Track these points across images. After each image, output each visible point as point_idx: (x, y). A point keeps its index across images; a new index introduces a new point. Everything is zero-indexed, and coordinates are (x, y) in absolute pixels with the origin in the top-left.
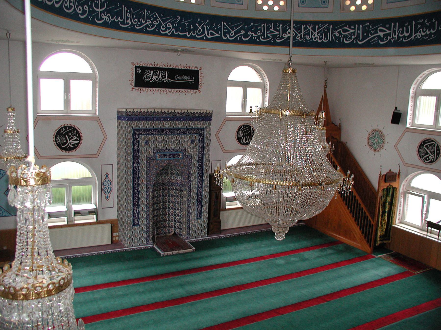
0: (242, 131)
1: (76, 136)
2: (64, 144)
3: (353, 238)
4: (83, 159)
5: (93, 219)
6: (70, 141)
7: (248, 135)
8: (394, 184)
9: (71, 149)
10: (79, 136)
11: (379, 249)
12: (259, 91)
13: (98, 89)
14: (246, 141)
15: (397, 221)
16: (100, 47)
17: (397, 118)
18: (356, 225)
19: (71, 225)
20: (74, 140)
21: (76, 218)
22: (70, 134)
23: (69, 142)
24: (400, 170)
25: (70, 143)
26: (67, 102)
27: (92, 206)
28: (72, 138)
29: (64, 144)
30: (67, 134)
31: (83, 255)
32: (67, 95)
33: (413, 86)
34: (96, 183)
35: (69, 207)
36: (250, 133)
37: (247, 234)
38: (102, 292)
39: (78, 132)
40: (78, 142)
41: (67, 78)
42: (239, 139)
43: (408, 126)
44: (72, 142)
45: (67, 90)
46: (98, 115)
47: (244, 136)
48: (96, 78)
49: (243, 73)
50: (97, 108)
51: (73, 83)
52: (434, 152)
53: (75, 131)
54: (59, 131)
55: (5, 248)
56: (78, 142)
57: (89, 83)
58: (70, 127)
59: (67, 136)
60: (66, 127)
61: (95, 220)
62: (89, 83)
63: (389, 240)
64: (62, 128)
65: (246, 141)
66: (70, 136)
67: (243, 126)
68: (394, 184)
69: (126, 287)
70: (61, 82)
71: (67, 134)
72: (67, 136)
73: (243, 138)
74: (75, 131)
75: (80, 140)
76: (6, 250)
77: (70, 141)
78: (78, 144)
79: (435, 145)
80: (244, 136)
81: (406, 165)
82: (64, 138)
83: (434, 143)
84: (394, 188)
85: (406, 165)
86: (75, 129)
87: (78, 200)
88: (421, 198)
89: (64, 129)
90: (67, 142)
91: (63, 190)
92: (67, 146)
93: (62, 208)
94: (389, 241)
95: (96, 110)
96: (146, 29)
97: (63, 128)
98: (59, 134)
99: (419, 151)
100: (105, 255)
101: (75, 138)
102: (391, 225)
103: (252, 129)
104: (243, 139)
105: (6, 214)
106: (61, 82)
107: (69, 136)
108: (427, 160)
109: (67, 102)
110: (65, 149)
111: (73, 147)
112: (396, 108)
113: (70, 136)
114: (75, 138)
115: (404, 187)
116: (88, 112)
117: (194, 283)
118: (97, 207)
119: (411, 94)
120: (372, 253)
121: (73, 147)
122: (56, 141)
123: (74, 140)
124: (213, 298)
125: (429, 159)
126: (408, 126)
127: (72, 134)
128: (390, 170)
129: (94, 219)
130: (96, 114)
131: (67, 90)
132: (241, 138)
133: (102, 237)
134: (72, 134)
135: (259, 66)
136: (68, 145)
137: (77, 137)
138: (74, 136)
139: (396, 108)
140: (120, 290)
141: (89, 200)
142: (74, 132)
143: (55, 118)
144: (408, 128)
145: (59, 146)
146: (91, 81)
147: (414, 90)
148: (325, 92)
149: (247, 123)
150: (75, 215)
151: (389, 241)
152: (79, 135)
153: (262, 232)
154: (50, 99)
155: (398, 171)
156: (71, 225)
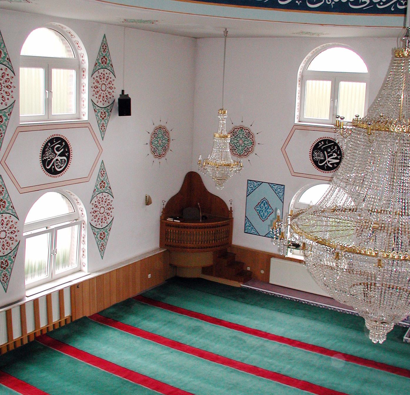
1: (336, 153)
2: (322, 161)
6: (329, 159)
9: (329, 169)
10: (340, 155)
12: (361, 88)
16: (355, 38)
20: (333, 159)
22: (329, 150)
23: (327, 160)
25: (329, 161)
28: (332, 155)
29: (322, 161)
30: (326, 149)
31: (343, 311)
38: (285, 348)
39: (339, 148)
40: (338, 161)
44: (331, 160)
49: (340, 58)
53: (336, 147)
54: (317, 145)
55: (249, 269)
56: (338, 161)
58: (330, 141)
59: (325, 152)
60: (325, 141)
64: (320, 142)
66: (329, 152)
69: (305, 352)
70: (328, 84)
71: (326, 149)
72: (325, 152)
74: (336, 147)
75: (340, 159)
76: (248, 271)
77: (329, 159)
78: (338, 164)
82: (322, 155)
86: (336, 144)
88: (58, 231)
89: (322, 142)
90: (325, 159)
92: (324, 165)
96: (395, 7)
97: (322, 141)
98: (316, 148)
101: (335, 155)
106: (328, 84)
107: (328, 153)
110: (322, 168)
111: (331, 166)
112: (123, 91)
113: (329, 152)
114: (335, 155)
116: (320, 121)
117: (306, 364)
119: (299, 76)
121: (331, 166)
122: (313, 157)
123: (333, 159)
124: (243, 373)
127: (332, 150)
134: (332, 150)
136: (326, 163)
137: (338, 155)
138: (334, 152)
139: (123, 91)
142: (334, 148)
143: (314, 129)
145: (316, 162)
147: (301, 71)
149: (330, 135)
152: (340, 152)
154: (315, 106)
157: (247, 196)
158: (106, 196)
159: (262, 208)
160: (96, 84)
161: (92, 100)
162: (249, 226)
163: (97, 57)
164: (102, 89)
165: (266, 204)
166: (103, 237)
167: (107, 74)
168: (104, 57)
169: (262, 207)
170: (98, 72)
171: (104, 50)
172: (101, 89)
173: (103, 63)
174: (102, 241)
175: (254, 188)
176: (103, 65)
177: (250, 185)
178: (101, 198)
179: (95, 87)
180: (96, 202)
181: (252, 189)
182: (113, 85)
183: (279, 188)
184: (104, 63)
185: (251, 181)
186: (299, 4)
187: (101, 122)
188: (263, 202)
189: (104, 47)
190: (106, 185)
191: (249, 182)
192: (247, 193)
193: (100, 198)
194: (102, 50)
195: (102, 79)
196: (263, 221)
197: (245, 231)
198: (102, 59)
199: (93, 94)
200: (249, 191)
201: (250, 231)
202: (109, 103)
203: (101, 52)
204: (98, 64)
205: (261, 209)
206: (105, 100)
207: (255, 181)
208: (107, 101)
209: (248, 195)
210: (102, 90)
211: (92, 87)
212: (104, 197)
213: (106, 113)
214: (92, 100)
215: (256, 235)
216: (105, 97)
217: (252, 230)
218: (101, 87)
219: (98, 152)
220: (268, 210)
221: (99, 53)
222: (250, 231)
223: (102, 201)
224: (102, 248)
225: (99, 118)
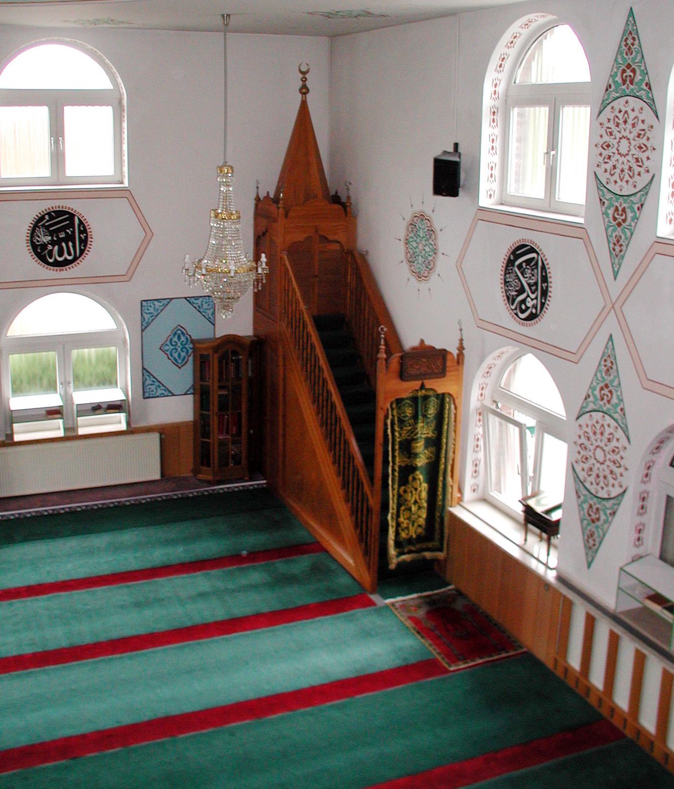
0: (47, 228)
3: (341, 541)
4: (95, 285)
5: (118, 422)
7: (66, 240)
8: (441, 386)
11: (388, 579)
13: (125, 125)
14: (61, 253)
15: (468, 494)
17: (448, 177)
18: (343, 503)
19: (71, 436)
21: (81, 420)
24: (461, 340)
26: (58, 157)
27: (114, 395)
31: (86, 506)
32: (57, 142)
33: (491, 76)
34: (125, 342)
35: (67, 398)
36: (73, 232)
37: (72, 513)
41: (56, 102)
42: (40, 252)
43: (485, 201)
45: (57, 130)
46: (126, 184)
47: (53, 243)
48: (120, 102)
50: (126, 169)
51: (71, 114)
52: (536, 284)
57: (107, 112)
61: (123, 427)
62: (107, 112)
63: (441, 550)
65: (61, 253)
67: (49, 214)
68: (441, 386)
70: (42, 113)
73: (50, 247)
79: (537, 264)
80: (53, 243)
81: (483, 324)
83: (534, 255)
84: (441, 398)
85: (483, 324)
87: (81, 382)
91: (52, 356)
93: (53, 400)
94: (441, 555)
95: (122, 172)
99: (506, 282)
100: (153, 504)
102: (443, 506)
103: (81, 222)
104: (51, 251)
105: (163, 392)
106: (42, 113)
108: (523, 312)
109: (58, 157)
115: (487, 392)
118: (127, 395)
119: (487, 102)
120: (373, 591)
125: (527, 308)
126: (485, 201)
128: (422, 341)
129: (120, 422)
130: (122, 183)
131: (57, 130)
132: (44, 246)
133: (142, 464)
135: (80, 40)
140: (166, 585)
141: (107, 381)
144: (483, 209)
146: (65, 108)
148: (304, 107)
150: (78, 416)
151: (441, 555)
153: (120, 507)
155: (457, 344)
156: (71, 436)
157: (142, 331)
158: (637, 110)
159: (176, 345)
160: (606, 138)
161: (595, 174)
162: (152, 385)
163: (592, 383)
164: (603, 453)
165: (182, 336)
166: (628, 71)
167: (633, 110)
168: (619, 225)
169: (174, 344)
170: (591, 416)
171: (618, 241)
172: (616, 152)
173: (597, 509)
174: (629, 59)
175: (155, 314)
176: (624, 87)
177: (148, 309)
178: (622, 113)
179: (604, 146)
180: (609, 120)
181: (151, 315)
182: (648, 139)
183: (152, 391)
184: (620, 209)
185: (149, 302)
186: (70, 233)
187: (614, 231)
188: (175, 333)
189: (630, 39)
190: (638, 77)
191: (144, 303)
192: (142, 324)
193: (620, 111)
194: (604, 369)
195: (622, 126)
196: (180, 368)
197: (144, 395)
198: (624, 71)
199: (597, 142)
200: (147, 320)
201: (205, 300)
202: (635, 186)
203: (601, 371)
204: (613, 86)
205: (172, 347)
206: (625, 180)
207: (155, 300)
208: (631, 181)
209: (143, 328)
210: (619, 154)
211: (596, 146)
212: (630, 112)
213: (628, 211)
214: (595, 174)
215: (167, 396)
216: (626, 171)
217: (159, 389)
218: (616, 145)
219: (603, 306)
220: (186, 346)
221: (595, 375)
222: (205, 300)
223: (625, 122)
224: (630, 41)
225: (609, 222)
